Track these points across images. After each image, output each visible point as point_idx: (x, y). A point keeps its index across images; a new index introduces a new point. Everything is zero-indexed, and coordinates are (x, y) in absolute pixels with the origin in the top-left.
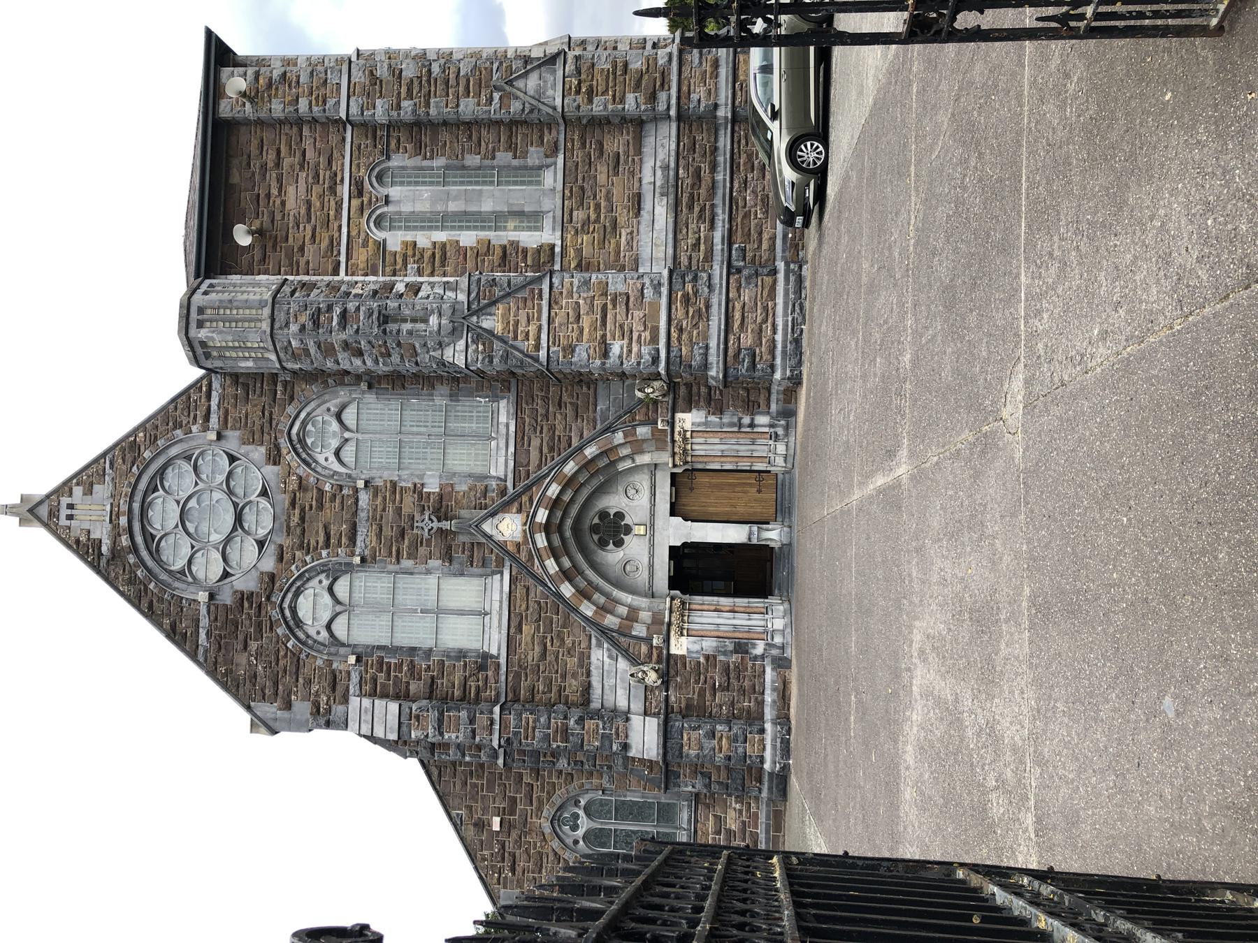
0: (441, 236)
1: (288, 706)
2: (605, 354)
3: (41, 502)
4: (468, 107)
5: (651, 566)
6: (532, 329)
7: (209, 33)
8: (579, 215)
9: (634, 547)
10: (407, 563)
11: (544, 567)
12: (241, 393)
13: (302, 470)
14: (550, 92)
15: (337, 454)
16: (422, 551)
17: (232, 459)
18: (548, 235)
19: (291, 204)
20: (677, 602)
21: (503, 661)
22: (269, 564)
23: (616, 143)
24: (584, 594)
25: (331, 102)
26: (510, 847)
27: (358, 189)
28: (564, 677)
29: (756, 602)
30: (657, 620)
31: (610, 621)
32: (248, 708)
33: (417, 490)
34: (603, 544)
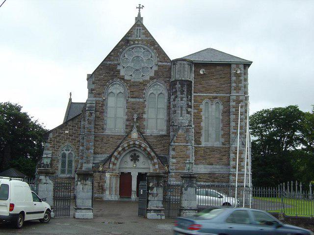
1: (93, 83)
3: (141, 22)
5: (127, 168)
7: (252, 62)
8: (208, 151)
9: (131, 164)
10: (126, 110)
12: (166, 68)
16: (129, 114)
17: (151, 68)
18: (203, 144)
19: (211, 81)
20: (118, 174)
21: (104, 134)
23: (225, 159)
24: (119, 153)
25: (235, 91)
27: (216, 98)
29: (118, 193)
30: (113, 170)
31: (113, 159)
33: (144, 113)
34: (132, 156)
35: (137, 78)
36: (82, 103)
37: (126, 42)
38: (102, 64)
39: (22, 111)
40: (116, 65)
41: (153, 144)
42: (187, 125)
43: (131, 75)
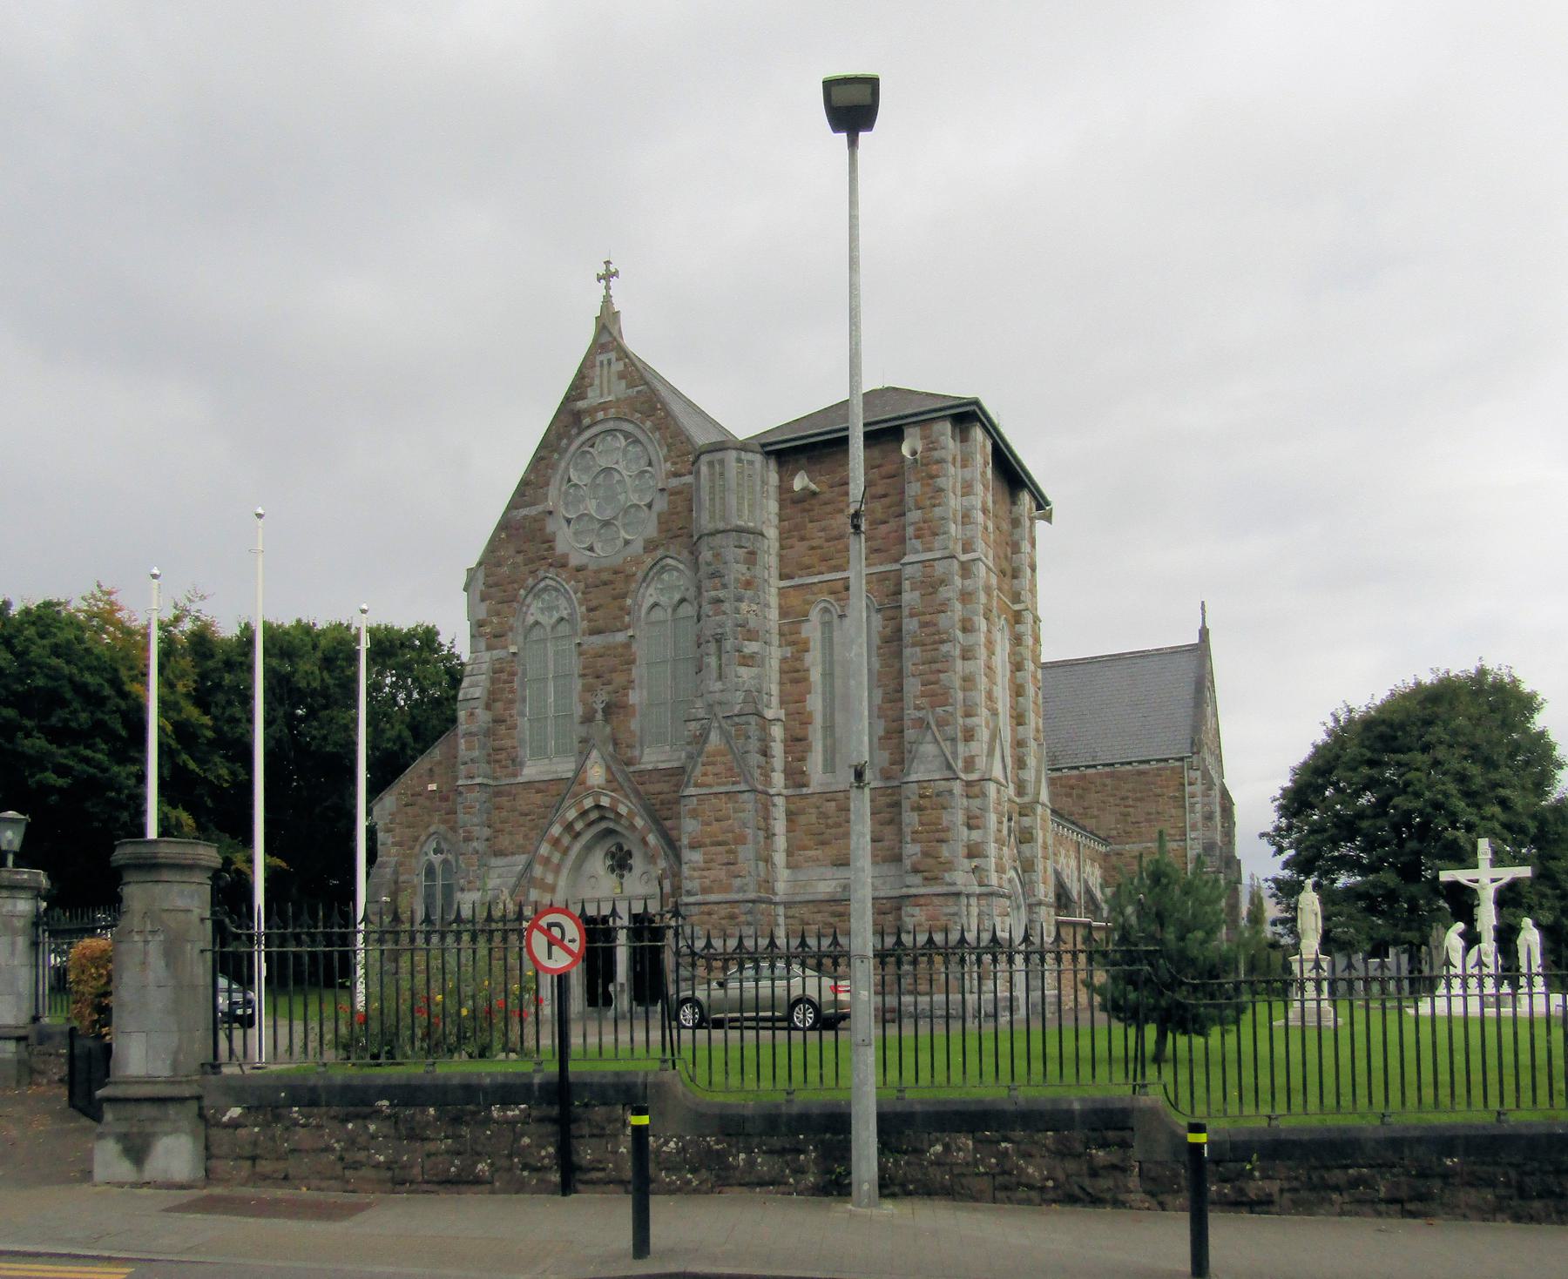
0: (816, 675)
2: (693, 847)
4: (912, 687)
6: (709, 780)
11: (570, 807)
13: (640, 575)
14: (922, 768)
15: (655, 605)
17: (650, 506)
22: (574, 561)
26: (421, 800)
28: (511, 833)
31: (538, 871)
32: (480, 564)
35: (606, 553)
36: (1175, 651)
37: (571, 419)
38: (504, 525)
39: (1539, 722)
40: (540, 519)
41: (662, 803)
42: (737, 710)
43: (591, 549)
